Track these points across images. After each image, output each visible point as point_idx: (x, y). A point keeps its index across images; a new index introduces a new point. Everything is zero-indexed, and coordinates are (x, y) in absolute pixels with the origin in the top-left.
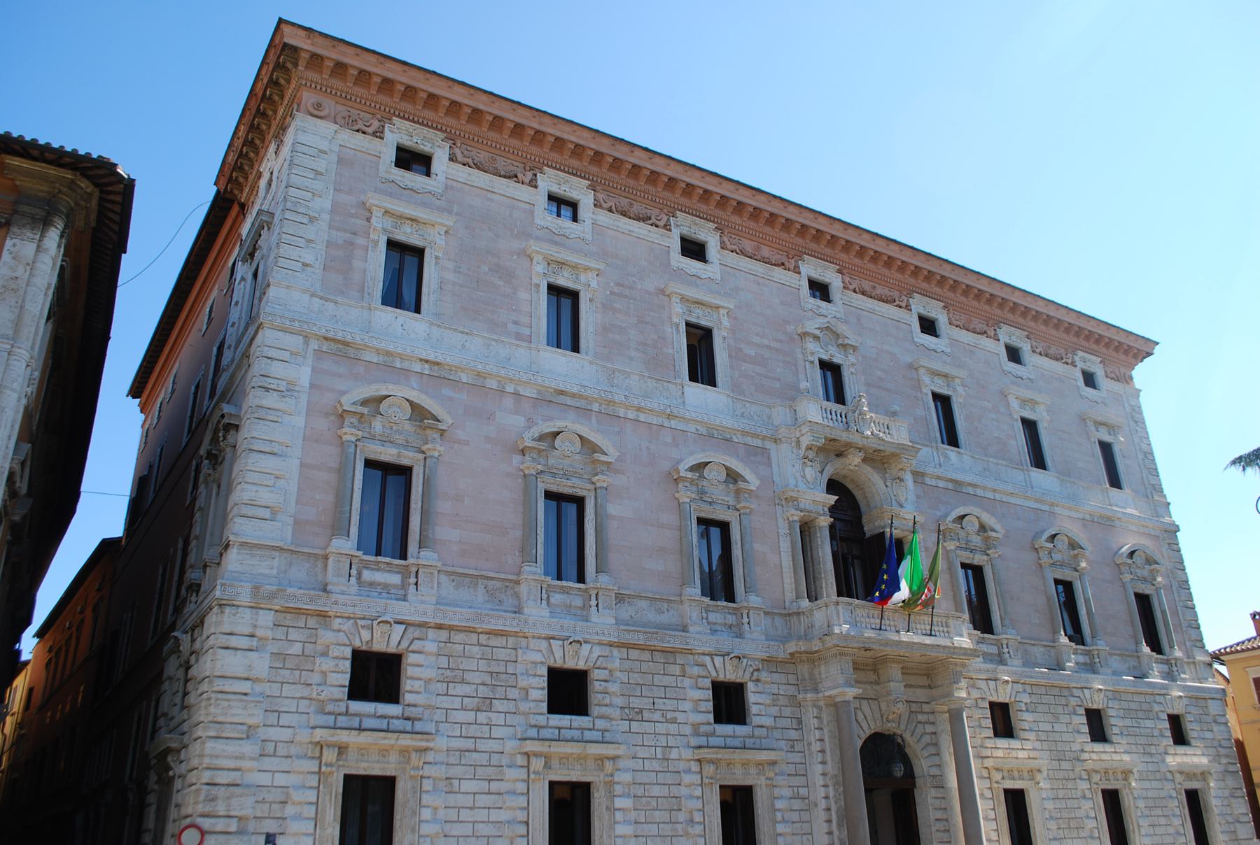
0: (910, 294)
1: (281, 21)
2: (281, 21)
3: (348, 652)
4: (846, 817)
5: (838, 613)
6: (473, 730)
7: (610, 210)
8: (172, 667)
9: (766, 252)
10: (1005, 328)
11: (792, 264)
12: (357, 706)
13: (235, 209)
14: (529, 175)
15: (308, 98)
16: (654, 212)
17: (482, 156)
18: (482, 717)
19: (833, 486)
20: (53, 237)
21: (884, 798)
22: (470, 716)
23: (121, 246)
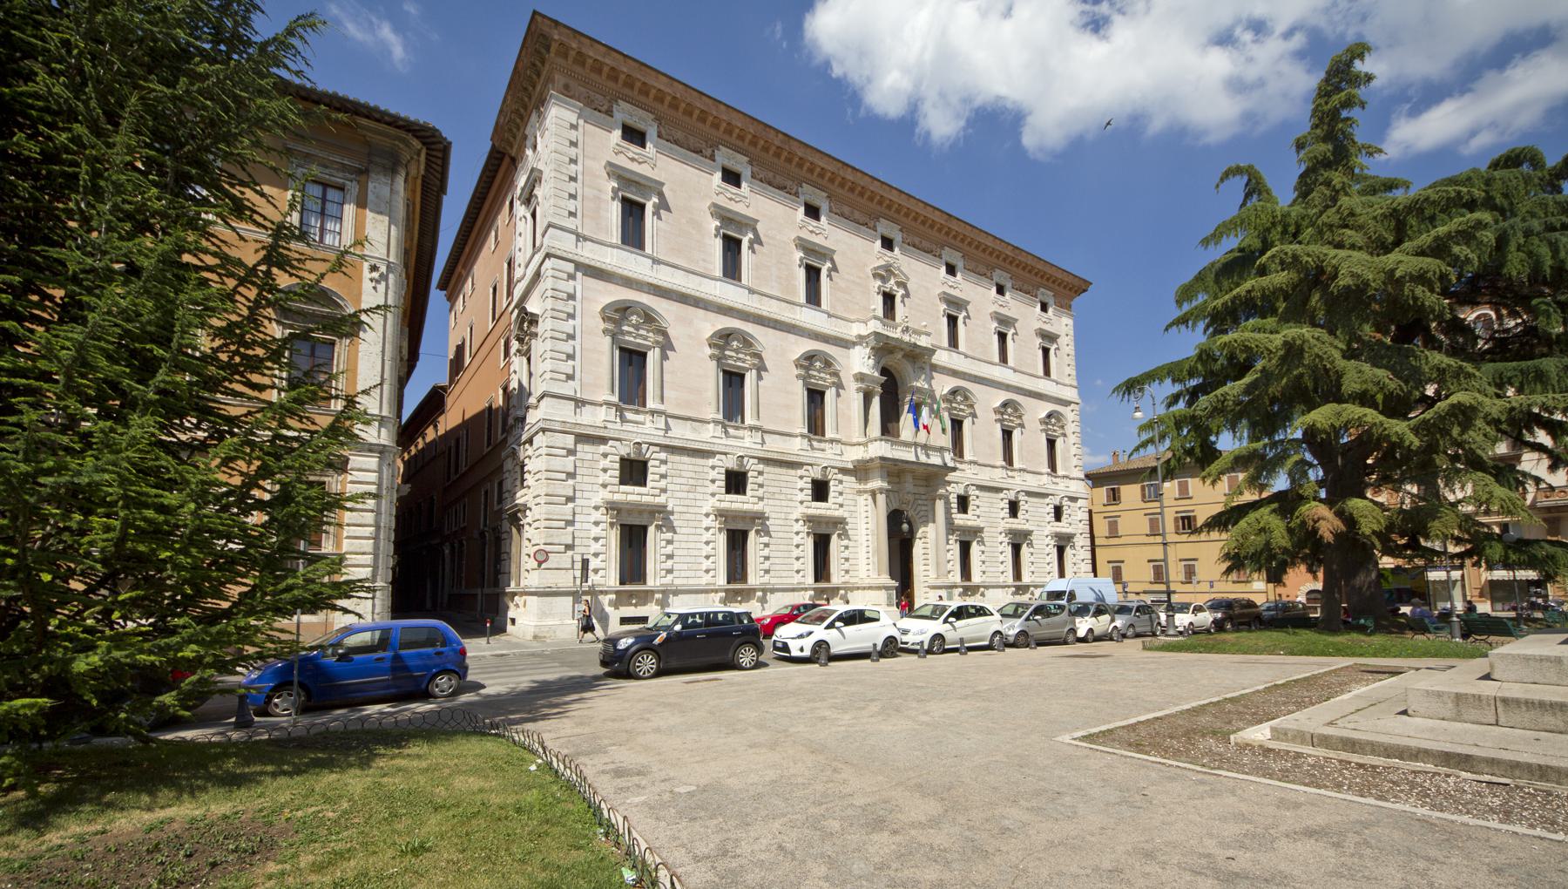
0: (942, 248)
1: (535, 13)
2: (535, 13)
3: (617, 458)
4: (878, 551)
5: (346, 611)
6: (686, 502)
7: (971, 406)
8: (508, 465)
9: (857, 215)
10: (998, 271)
11: (871, 224)
12: (623, 488)
13: (507, 160)
14: (709, 151)
15: (560, 79)
16: (789, 183)
17: (679, 135)
18: (691, 495)
19: (884, 371)
20: (400, 181)
21: (896, 542)
22: (684, 495)
23: (442, 189)
